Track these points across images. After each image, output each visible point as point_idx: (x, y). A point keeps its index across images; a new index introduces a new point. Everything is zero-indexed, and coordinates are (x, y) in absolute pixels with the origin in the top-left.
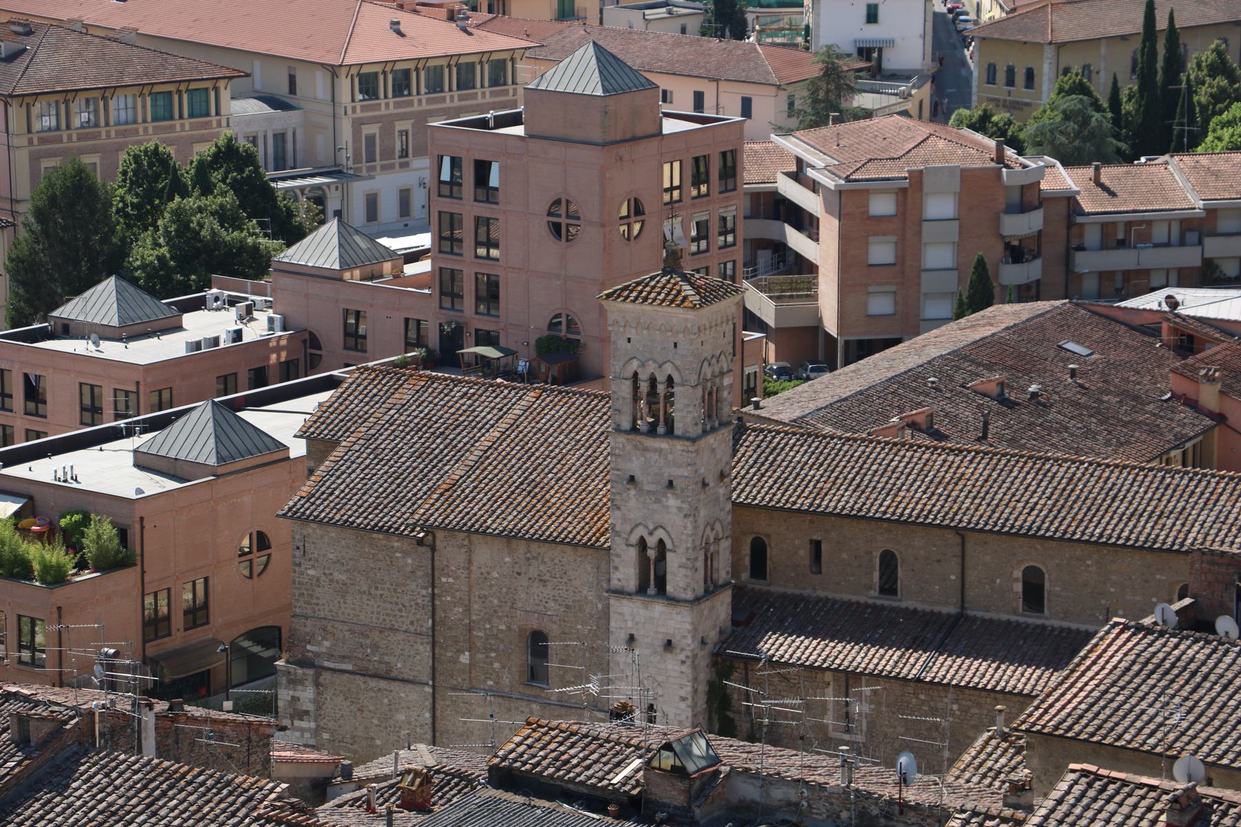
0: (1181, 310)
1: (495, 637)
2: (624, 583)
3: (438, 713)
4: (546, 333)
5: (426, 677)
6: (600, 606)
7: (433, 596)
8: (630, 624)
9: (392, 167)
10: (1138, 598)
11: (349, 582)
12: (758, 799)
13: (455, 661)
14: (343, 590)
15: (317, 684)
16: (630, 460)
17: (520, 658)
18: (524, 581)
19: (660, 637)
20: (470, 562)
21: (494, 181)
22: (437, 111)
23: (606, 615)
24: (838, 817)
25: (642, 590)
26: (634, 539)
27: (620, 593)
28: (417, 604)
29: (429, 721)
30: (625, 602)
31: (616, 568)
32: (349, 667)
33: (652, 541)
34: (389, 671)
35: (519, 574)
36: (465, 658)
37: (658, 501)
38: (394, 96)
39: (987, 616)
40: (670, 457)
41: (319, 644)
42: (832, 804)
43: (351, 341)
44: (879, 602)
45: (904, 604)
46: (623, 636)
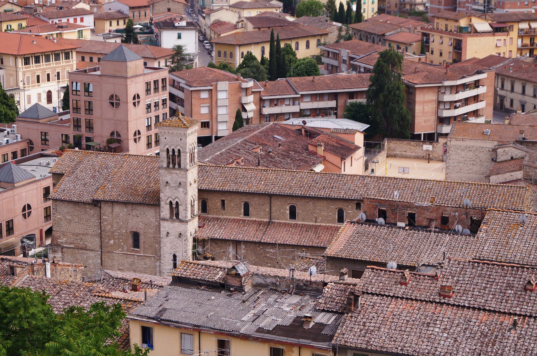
0: (307, 125)
1: (122, 235)
2: (165, 216)
3: (103, 259)
4: (109, 138)
5: (98, 249)
6: (157, 223)
7: (101, 222)
8: (167, 229)
9: (35, 86)
10: (325, 213)
11: (71, 219)
12: (263, 283)
13: (108, 243)
14: (70, 221)
15: (62, 252)
16: (167, 177)
17: (130, 241)
18: (131, 216)
19: (177, 232)
20: (113, 211)
21: (91, 89)
22: (526, 49)
23: (159, 226)
24: (289, 287)
25: (171, 217)
26: (168, 202)
27: (164, 219)
28: (95, 225)
29: (100, 262)
30: (165, 222)
31: (162, 212)
32: (73, 246)
33: (174, 202)
34: (86, 247)
35: (129, 214)
36: (112, 242)
37: (176, 189)
38: (45, 62)
39: (278, 221)
40: (180, 175)
41: (62, 239)
42: (287, 283)
43: (44, 142)
44: (244, 219)
45: (252, 219)
46: (165, 233)
